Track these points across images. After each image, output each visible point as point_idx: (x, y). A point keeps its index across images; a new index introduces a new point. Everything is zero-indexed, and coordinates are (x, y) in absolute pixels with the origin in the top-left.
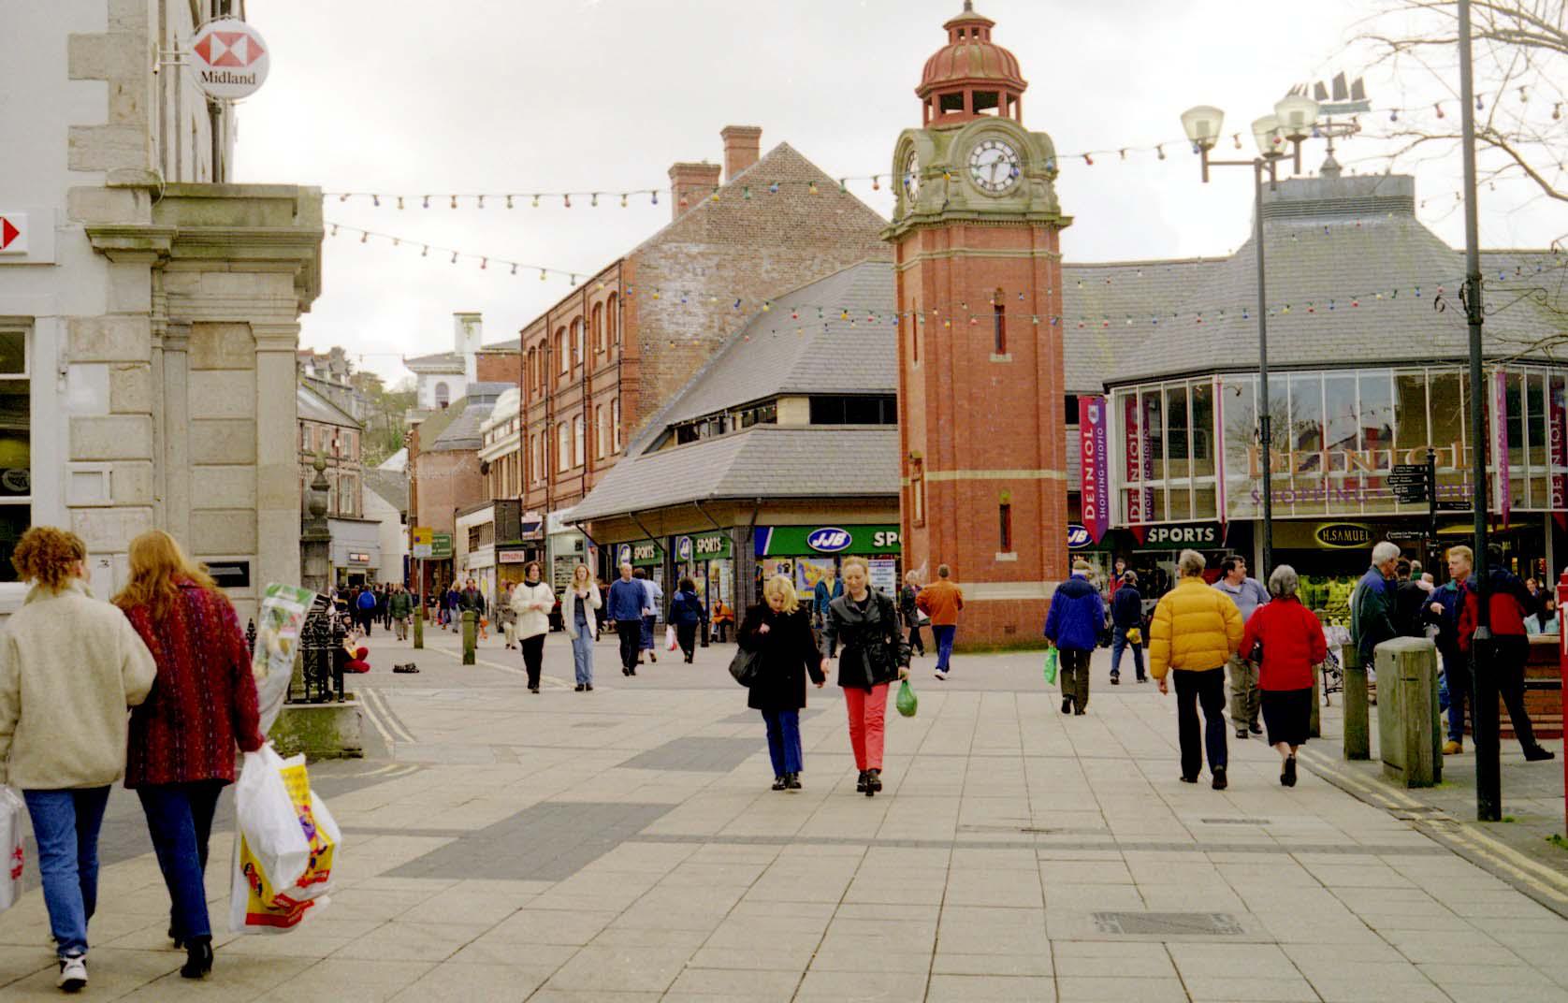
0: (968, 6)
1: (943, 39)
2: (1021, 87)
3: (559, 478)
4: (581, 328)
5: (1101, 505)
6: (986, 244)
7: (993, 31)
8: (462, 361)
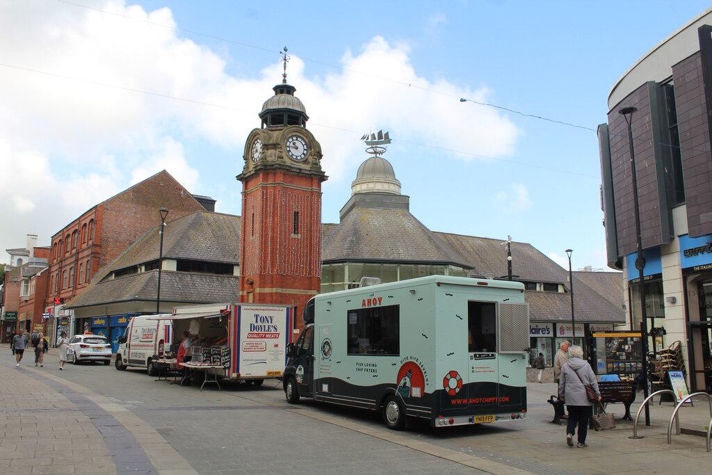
2: (306, 118)
3: (62, 292)
4: (77, 234)
5: (54, 312)
6: (291, 182)
8: (29, 252)
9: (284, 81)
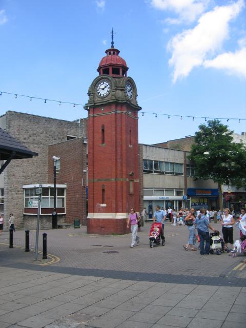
1: (105, 55)
9: (113, 46)
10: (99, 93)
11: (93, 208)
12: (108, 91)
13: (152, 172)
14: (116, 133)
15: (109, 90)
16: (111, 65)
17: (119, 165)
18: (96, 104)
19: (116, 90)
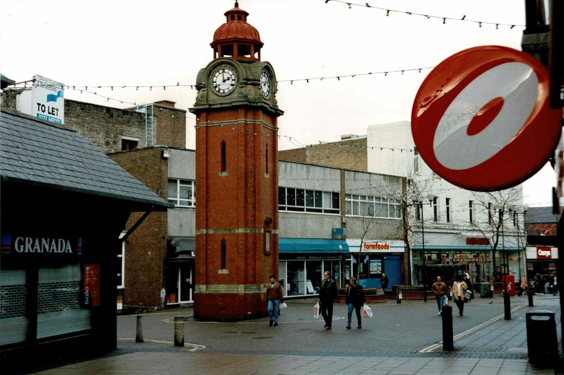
0: (237, 5)
1: (224, 20)
2: (261, 45)
7: (248, 18)
10: (220, 89)
11: (207, 207)
12: (232, 85)
13: (302, 210)
14: (246, 156)
15: (233, 82)
16: (236, 40)
17: (250, 207)
18: (212, 107)
19: (246, 84)
